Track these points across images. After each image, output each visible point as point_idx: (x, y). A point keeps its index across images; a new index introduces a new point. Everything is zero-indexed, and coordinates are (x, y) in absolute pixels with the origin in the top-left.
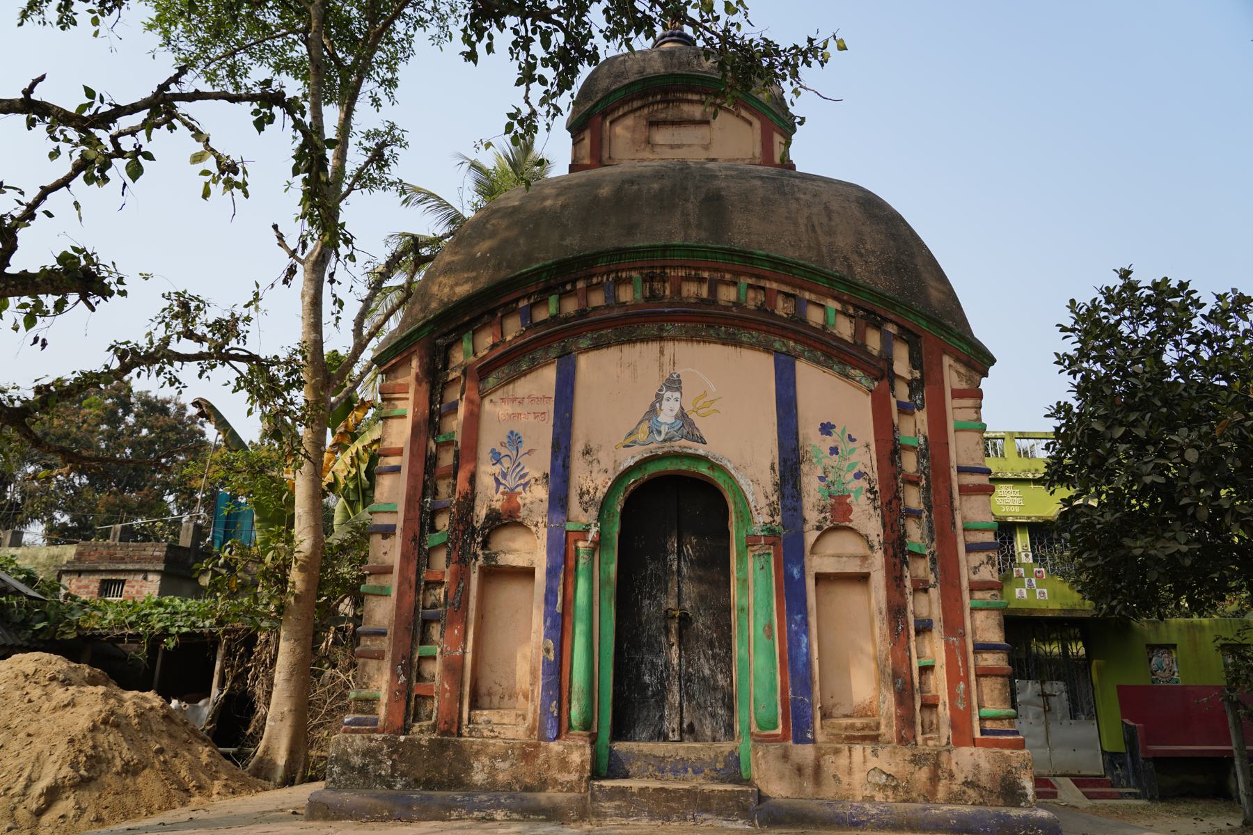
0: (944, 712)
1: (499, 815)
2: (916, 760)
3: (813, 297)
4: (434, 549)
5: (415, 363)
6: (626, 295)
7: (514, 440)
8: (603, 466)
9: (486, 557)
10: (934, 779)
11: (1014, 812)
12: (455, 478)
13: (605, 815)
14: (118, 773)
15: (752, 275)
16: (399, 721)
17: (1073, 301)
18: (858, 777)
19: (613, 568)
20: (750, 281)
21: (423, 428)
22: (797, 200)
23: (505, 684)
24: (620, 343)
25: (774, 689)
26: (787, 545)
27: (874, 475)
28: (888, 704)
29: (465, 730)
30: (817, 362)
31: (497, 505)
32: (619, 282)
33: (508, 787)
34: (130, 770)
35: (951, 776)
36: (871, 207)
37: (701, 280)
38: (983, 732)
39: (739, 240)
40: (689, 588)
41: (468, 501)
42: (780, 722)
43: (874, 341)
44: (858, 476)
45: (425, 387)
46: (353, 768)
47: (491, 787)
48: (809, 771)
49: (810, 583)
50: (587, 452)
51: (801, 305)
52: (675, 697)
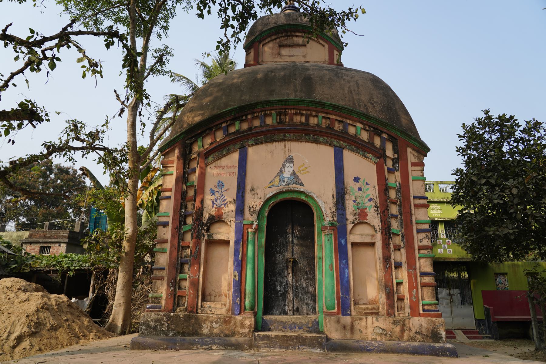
0: (407, 302)
1: (214, 347)
2: (395, 323)
3: (351, 122)
4: (186, 232)
5: (177, 151)
6: (269, 121)
7: (221, 184)
8: (259, 196)
9: (208, 236)
10: (403, 331)
11: (437, 345)
12: (195, 201)
13: (260, 347)
14: (48, 330)
15: (324, 113)
16: (171, 307)
17: (464, 124)
18: (370, 330)
19: (264, 240)
20: (323, 115)
23: (217, 291)
24: (267, 142)
25: (333, 292)
26: (339, 230)
27: (377, 200)
28: (383, 299)
29: (199, 311)
30: (353, 151)
31: (213, 213)
32: (266, 115)
33: (218, 335)
34: (54, 328)
37: (302, 115)
38: (424, 311)
39: (318, 97)
40: (297, 249)
41: (201, 211)
42: (336, 307)
43: (377, 141)
44: (370, 200)
45: (181, 161)
46: (151, 327)
47: (211, 335)
48: (348, 328)
50: (252, 190)
51: (345, 125)
52: (290, 296)
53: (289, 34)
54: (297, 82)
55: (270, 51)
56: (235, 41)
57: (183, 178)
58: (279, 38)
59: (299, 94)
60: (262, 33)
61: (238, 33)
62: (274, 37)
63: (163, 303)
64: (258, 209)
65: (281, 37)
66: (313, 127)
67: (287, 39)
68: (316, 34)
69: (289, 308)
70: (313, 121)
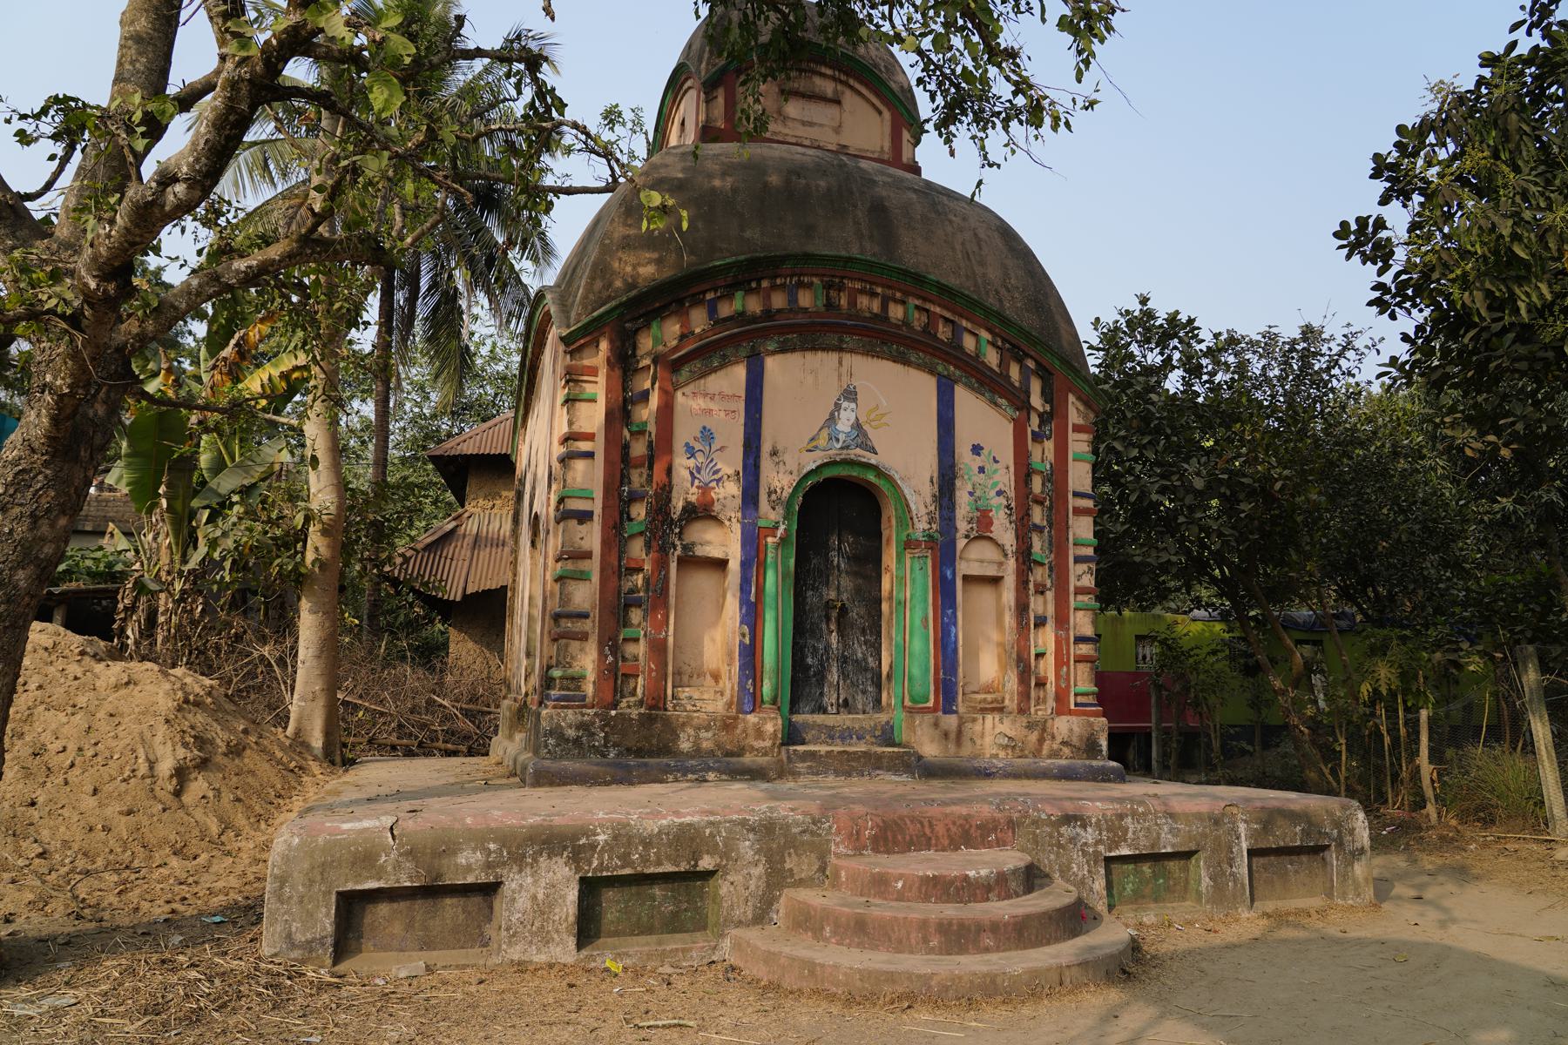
0: (1051, 688)
1: (711, 776)
2: (1030, 726)
3: (969, 326)
4: (632, 537)
5: (604, 345)
6: (805, 299)
7: (707, 435)
8: (788, 468)
9: (685, 547)
10: (1041, 741)
11: (1094, 763)
12: (651, 468)
13: (799, 774)
14: (225, 755)
15: (919, 297)
16: (609, 697)
17: (1097, 319)
18: (988, 740)
19: (792, 561)
20: (917, 302)
21: (617, 414)
22: (951, 222)
23: (693, 665)
24: (804, 349)
25: (927, 670)
26: (943, 550)
27: (1012, 494)
28: (1012, 682)
29: (669, 706)
30: (973, 389)
31: (693, 499)
32: (800, 285)
33: (711, 753)
34: (235, 751)
35: (1053, 737)
36: (1007, 234)
37: (873, 295)
38: (1076, 705)
39: (910, 261)
40: (846, 582)
41: (666, 491)
42: (932, 697)
43: (1014, 372)
44: (999, 493)
45: (618, 372)
46: (567, 740)
47: (697, 752)
48: (953, 736)
49: (959, 583)
50: (774, 453)
51: (957, 331)
52: (834, 676)
53: (804, 66)
57: (620, 414)
59: (868, 245)
63: (589, 689)
64: (786, 494)
66: (897, 326)
69: (830, 698)
70: (896, 312)
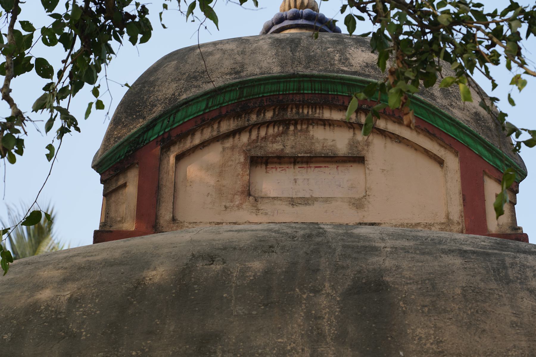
53: (290, 114)
54: (323, 301)
55: (212, 181)
56: (49, 126)
58: (249, 128)
60: (175, 108)
61: (64, 93)
62: (226, 126)
65: (258, 126)
67: (285, 133)
68: (401, 92)
